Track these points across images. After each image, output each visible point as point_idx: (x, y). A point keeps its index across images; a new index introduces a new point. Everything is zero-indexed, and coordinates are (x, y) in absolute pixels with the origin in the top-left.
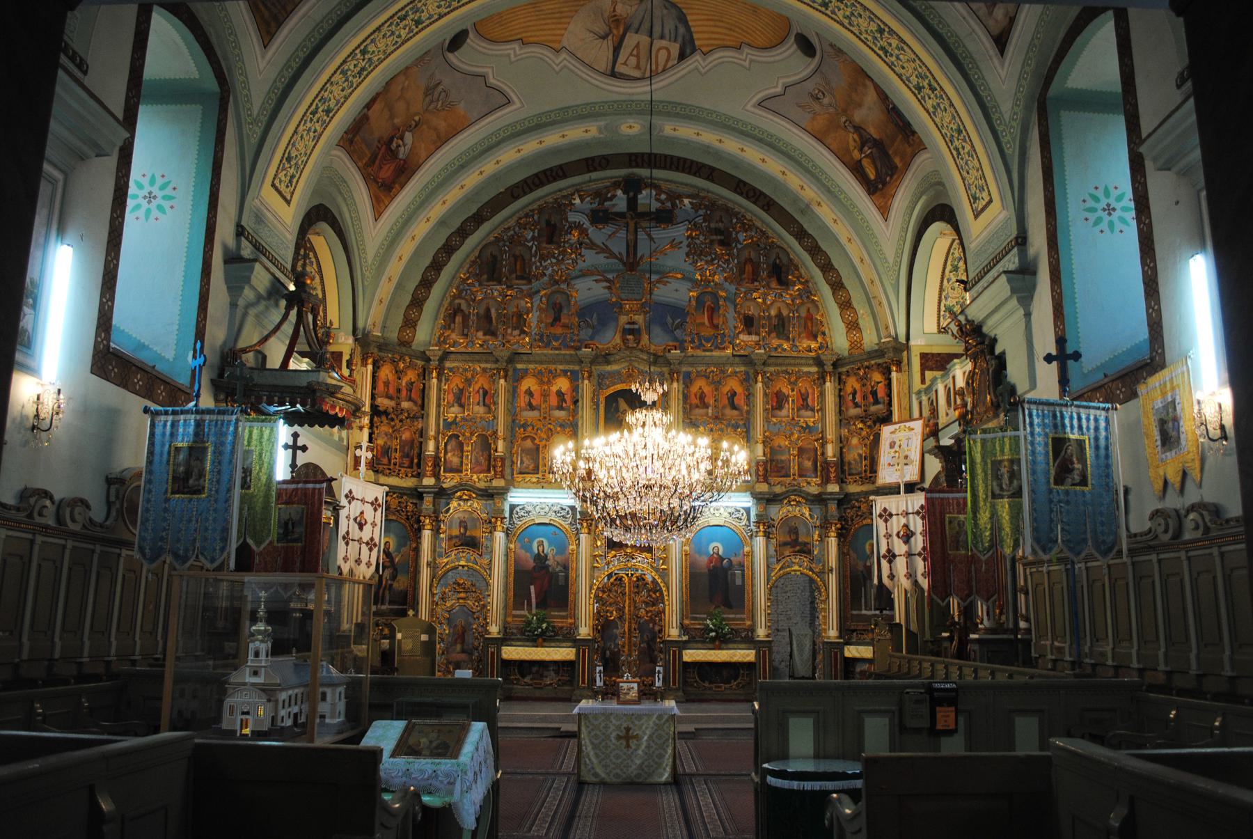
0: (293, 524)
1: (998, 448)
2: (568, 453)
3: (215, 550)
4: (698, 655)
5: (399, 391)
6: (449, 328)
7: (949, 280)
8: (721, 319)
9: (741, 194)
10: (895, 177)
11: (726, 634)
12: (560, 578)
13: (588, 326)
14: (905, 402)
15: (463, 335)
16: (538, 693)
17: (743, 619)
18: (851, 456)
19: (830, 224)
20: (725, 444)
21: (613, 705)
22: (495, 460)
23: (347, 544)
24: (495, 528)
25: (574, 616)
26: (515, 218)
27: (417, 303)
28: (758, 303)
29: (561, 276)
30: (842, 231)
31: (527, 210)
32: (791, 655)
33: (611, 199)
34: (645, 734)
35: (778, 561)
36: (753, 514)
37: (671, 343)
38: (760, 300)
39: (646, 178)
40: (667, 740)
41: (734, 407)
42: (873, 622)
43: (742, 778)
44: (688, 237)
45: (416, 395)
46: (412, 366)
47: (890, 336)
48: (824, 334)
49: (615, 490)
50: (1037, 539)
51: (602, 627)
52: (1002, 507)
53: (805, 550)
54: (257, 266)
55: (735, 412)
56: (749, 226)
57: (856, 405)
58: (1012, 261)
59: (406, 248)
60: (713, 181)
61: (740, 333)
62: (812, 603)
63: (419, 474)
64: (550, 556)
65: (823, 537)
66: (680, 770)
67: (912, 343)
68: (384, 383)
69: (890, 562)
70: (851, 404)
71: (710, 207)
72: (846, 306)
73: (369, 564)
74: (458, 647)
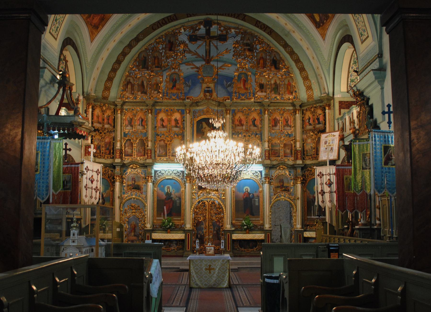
0: (67, 182)
1: (365, 148)
2: (182, 150)
3: (44, 195)
4: (239, 236)
5: (103, 120)
6: (125, 91)
7: (352, 68)
8: (249, 85)
9: (258, 27)
10: (328, 20)
11: (251, 227)
12: (177, 203)
13: (187, 86)
14: (332, 124)
15: (132, 93)
16: (168, 254)
17: (259, 221)
18: (307, 147)
19: (299, 41)
20: (250, 146)
21: (203, 256)
22: (147, 150)
23: (86, 189)
24: (148, 181)
25: (184, 219)
26: (154, 39)
27: (110, 79)
28: (266, 78)
29: (176, 66)
30: (304, 44)
31: (159, 35)
32: (281, 236)
33: (198, 30)
34: (217, 268)
35: (275, 194)
36: (263, 173)
37: (226, 97)
38: (267, 76)
39: (215, 20)
40: (226, 270)
41: (255, 125)
42: (315, 221)
43: (258, 286)
44: (234, 47)
45: (111, 121)
46: (109, 108)
47: (325, 93)
48: (296, 92)
49: (203, 166)
50: (376, 187)
51: (197, 224)
52: (366, 173)
53: (287, 190)
54: (46, 70)
55: (255, 128)
56: (262, 42)
57: (310, 124)
58: (376, 65)
59: (105, 54)
60: (245, 21)
61: (257, 91)
62: (290, 213)
63: (113, 157)
64: (173, 193)
65: (294, 184)
66: (232, 283)
67: (335, 96)
68: (97, 116)
69: (322, 195)
70: (308, 124)
71: (245, 33)
72: (306, 78)
73: (96, 198)
74: (133, 234)
